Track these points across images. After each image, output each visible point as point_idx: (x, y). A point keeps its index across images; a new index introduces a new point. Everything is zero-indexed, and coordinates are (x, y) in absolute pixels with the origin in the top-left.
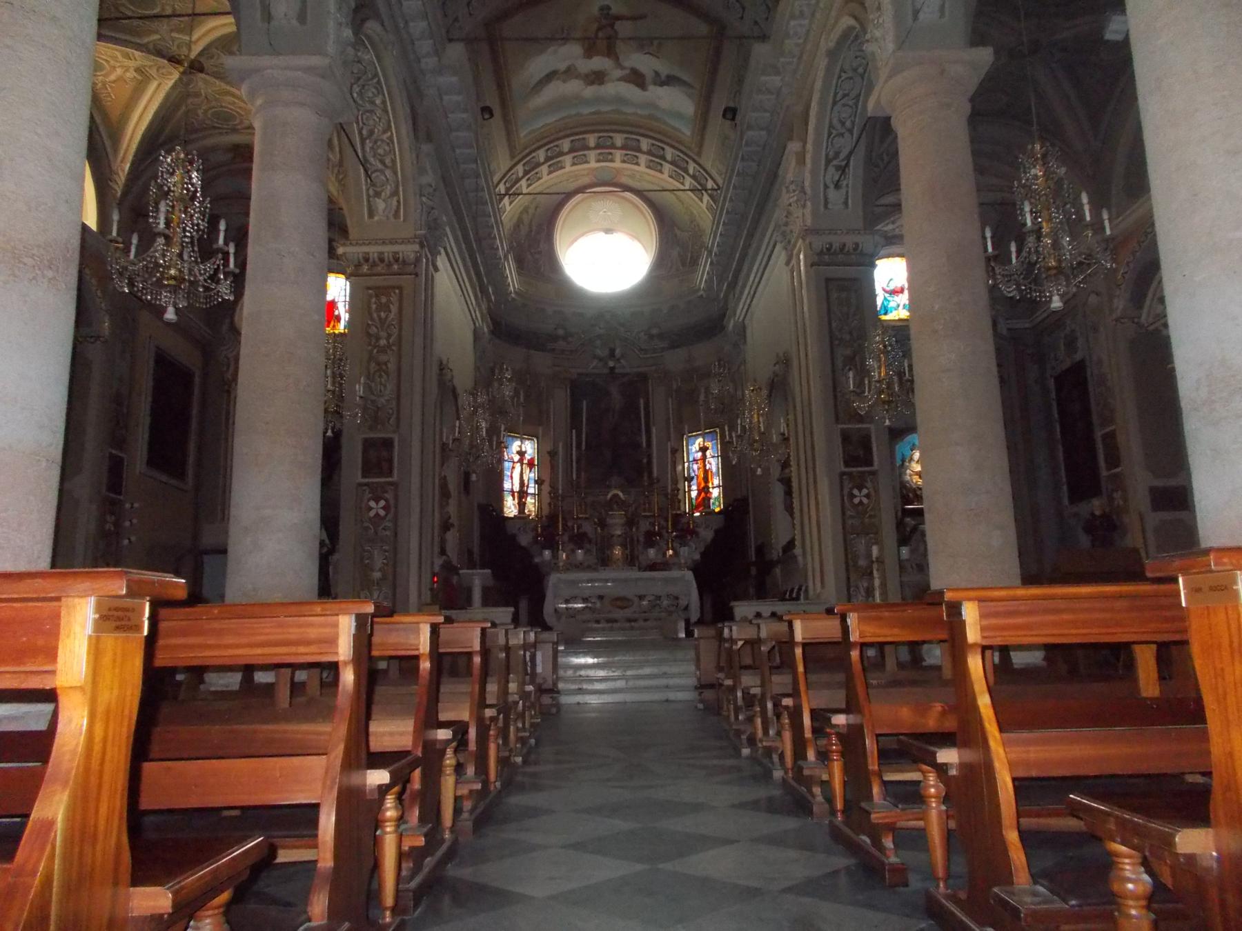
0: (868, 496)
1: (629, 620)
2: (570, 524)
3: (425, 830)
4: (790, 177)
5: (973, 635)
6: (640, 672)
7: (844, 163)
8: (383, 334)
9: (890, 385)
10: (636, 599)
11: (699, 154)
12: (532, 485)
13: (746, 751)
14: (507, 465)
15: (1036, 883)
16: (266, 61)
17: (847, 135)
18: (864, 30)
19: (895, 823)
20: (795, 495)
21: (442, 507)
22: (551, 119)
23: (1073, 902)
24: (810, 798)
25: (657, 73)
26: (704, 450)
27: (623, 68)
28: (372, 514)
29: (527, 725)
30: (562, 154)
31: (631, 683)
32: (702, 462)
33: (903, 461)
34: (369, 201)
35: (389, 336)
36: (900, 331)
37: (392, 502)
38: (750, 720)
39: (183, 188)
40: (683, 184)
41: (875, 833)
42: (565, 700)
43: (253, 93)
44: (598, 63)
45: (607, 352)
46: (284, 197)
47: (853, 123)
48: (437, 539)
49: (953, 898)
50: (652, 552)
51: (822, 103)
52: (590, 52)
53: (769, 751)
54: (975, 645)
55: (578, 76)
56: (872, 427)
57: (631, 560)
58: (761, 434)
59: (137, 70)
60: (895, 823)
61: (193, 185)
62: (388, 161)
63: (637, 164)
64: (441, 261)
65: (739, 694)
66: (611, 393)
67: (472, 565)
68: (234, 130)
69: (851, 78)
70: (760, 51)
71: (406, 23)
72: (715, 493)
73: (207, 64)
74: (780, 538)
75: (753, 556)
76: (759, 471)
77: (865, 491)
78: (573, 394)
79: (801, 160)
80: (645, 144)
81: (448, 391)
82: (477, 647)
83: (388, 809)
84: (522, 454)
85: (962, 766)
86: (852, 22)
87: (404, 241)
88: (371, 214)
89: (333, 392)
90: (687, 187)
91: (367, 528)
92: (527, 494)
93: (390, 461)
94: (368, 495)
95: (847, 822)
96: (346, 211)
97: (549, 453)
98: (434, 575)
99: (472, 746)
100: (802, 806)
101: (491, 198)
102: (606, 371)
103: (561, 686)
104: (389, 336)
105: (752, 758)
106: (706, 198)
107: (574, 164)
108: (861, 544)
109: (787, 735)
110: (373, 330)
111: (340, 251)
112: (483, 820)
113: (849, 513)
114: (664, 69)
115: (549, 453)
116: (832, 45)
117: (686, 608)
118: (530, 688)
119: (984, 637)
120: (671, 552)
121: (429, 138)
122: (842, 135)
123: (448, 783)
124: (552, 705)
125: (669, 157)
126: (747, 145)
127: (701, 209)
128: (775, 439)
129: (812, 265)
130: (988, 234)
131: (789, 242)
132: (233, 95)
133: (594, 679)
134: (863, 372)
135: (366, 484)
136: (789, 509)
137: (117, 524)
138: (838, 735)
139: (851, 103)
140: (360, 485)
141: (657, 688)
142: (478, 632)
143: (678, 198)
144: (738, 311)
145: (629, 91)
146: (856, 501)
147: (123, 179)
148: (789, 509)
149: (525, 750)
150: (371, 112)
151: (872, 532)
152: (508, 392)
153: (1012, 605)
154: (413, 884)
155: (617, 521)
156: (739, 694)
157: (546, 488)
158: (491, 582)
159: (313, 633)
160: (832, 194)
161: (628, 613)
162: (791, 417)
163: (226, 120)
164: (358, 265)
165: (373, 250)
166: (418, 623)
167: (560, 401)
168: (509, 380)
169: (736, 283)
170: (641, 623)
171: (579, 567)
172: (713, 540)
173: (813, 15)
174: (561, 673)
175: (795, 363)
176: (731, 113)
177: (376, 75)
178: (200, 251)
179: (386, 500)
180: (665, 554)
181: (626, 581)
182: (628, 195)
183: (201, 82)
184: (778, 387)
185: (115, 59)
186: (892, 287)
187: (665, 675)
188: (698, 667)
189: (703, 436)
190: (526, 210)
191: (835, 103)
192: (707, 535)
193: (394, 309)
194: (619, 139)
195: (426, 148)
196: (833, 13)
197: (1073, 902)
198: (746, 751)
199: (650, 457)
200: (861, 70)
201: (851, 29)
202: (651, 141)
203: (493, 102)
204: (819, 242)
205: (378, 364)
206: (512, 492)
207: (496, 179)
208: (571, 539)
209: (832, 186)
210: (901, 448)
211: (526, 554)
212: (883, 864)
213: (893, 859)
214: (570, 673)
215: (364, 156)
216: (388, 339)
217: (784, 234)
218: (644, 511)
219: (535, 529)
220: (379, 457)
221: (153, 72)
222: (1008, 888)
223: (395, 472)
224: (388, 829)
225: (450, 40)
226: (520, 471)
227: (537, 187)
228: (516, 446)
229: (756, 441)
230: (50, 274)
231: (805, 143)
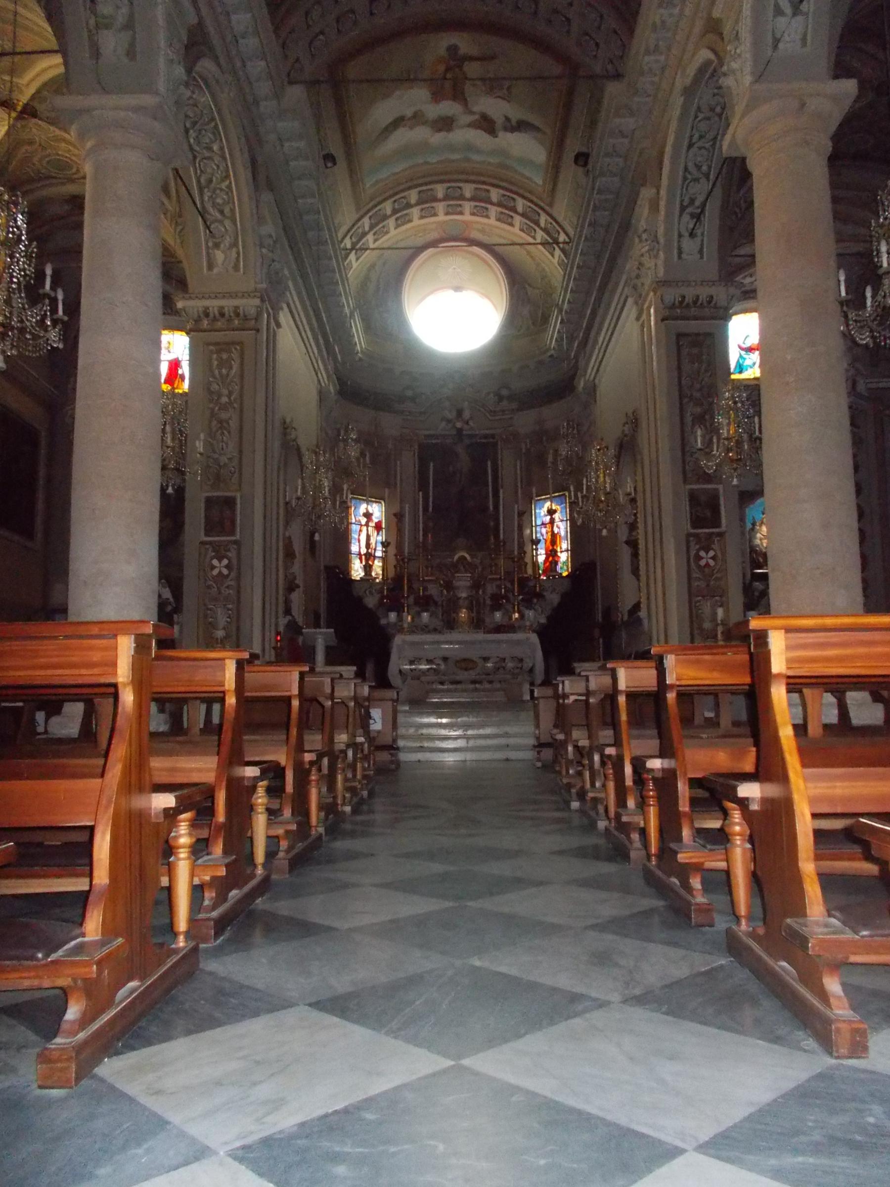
0: (713, 558)
1: (474, 682)
2: (415, 586)
3: (227, 861)
4: (643, 225)
5: (778, 665)
6: (481, 732)
7: (699, 210)
9: (739, 443)
10: (480, 663)
11: (551, 205)
12: (380, 548)
13: (575, 805)
14: (355, 528)
15: (830, 915)
16: (93, 100)
17: (703, 180)
18: (721, 64)
19: (703, 864)
20: (642, 558)
21: (286, 568)
22: (399, 168)
23: (865, 933)
24: (627, 843)
25: (508, 119)
26: (551, 512)
27: (472, 113)
28: (215, 572)
29: (359, 777)
30: (409, 206)
31: (472, 743)
32: (550, 525)
33: (754, 524)
34: (208, 254)
36: (753, 389)
37: (235, 561)
38: (580, 774)
39: (8, 232)
40: (534, 238)
41: (684, 872)
42: (403, 757)
43: (82, 136)
44: (448, 108)
45: (454, 413)
46: (119, 249)
47: (710, 167)
48: (281, 599)
49: (753, 935)
50: (498, 615)
51: (676, 148)
52: (437, 96)
53: (595, 800)
54: (779, 675)
55: (425, 123)
56: (721, 487)
57: (477, 624)
58: (607, 494)
60: (703, 864)
61: (18, 228)
62: (227, 211)
63: (487, 217)
64: (284, 317)
65: (570, 748)
66: (462, 459)
67: (317, 625)
68: (72, 181)
69: (708, 119)
70: (612, 88)
72: (563, 557)
73: (40, 107)
74: (626, 603)
75: (599, 617)
76: (604, 532)
77: (711, 553)
78: (421, 459)
79: (654, 207)
80: (495, 194)
81: (291, 449)
82: (295, 691)
83: (180, 836)
84: (368, 515)
85: (764, 801)
86: (712, 56)
88: (210, 267)
89: (173, 449)
90: (539, 241)
91: (209, 587)
92: (375, 557)
93: (233, 522)
95: (658, 866)
96: (185, 264)
97: (395, 515)
98: (278, 633)
99: (289, 788)
100: (620, 853)
101: (335, 252)
102: (454, 432)
103: (401, 743)
105: (582, 811)
106: (557, 252)
107: (422, 217)
108: (706, 608)
109: (611, 785)
110: (215, 387)
111: (180, 305)
112: (297, 862)
113: (694, 575)
114: (515, 113)
115: (395, 515)
116: (688, 81)
117: (531, 670)
118: (360, 739)
119: (788, 668)
120: (517, 615)
121: (271, 188)
122: (696, 180)
123: (260, 821)
124: (392, 762)
125: (520, 209)
126: (600, 192)
127: (551, 264)
128: (622, 499)
129: (663, 320)
130: (842, 278)
131: (640, 296)
132: (64, 140)
133: (446, 741)
134: (713, 430)
135: (210, 543)
136: (635, 571)
138: (654, 779)
139: (707, 145)
140: (203, 543)
141: (499, 748)
142: (296, 676)
143: (529, 253)
144: (589, 371)
145: (478, 137)
146: (703, 563)
148: (635, 571)
149: (355, 800)
150: (210, 158)
151: (717, 594)
152: (353, 452)
153: (821, 637)
154: (215, 914)
155: (463, 582)
156: (570, 748)
157: (392, 550)
158: (333, 642)
159: (96, 657)
160: (689, 245)
161: (472, 675)
162: (639, 478)
163: (64, 170)
164: (198, 321)
165: (214, 304)
166: (224, 659)
167: (407, 464)
168: (356, 441)
169: (587, 341)
170: (487, 686)
171: (426, 629)
172: (559, 604)
173: (669, 49)
174: (402, 731)
175: (644, 425)
176: (582, 159)
177: (213, 119)
178: (27, 297)
179: (229, 560)
180: (511, 618)
181: (473, 643)
182: (475, 249)
184: (627, 448)
186: (748, 344)
187: (506, 735)
188: (537, 726)
189: (551, 499)
190: (373, 266)
191: (690, 146)
192: (554, 598)
194: (468, 190)
195: (267, 197)
196: (690, 47)
197: (865, 933)
198: (575, 805)
199: (497, 520)
200: (718, 110)
201: (707, 63)
202: (502, 192)
203: (338, 152)
204: (671, 295)
205: (220, 422)
206: (360, 554)
207: (340, 235)
208: (416, 603)
209: (687, 234)
210: (753, 511)
211: (371, 616)
212: (689, 904)
213: (700, 899)
214: (412, 731)
215: (204, 207)
217: (635, 287)
218: (491, 573)
219: (381, 592)
220: (222, 515)
222: (801, 920)
224: (182, 856)
225: (291, 83)
226: (368, 532)
227: (383, 241)
228: (363, 508)
229: (602, 501)
231: (658, 189)
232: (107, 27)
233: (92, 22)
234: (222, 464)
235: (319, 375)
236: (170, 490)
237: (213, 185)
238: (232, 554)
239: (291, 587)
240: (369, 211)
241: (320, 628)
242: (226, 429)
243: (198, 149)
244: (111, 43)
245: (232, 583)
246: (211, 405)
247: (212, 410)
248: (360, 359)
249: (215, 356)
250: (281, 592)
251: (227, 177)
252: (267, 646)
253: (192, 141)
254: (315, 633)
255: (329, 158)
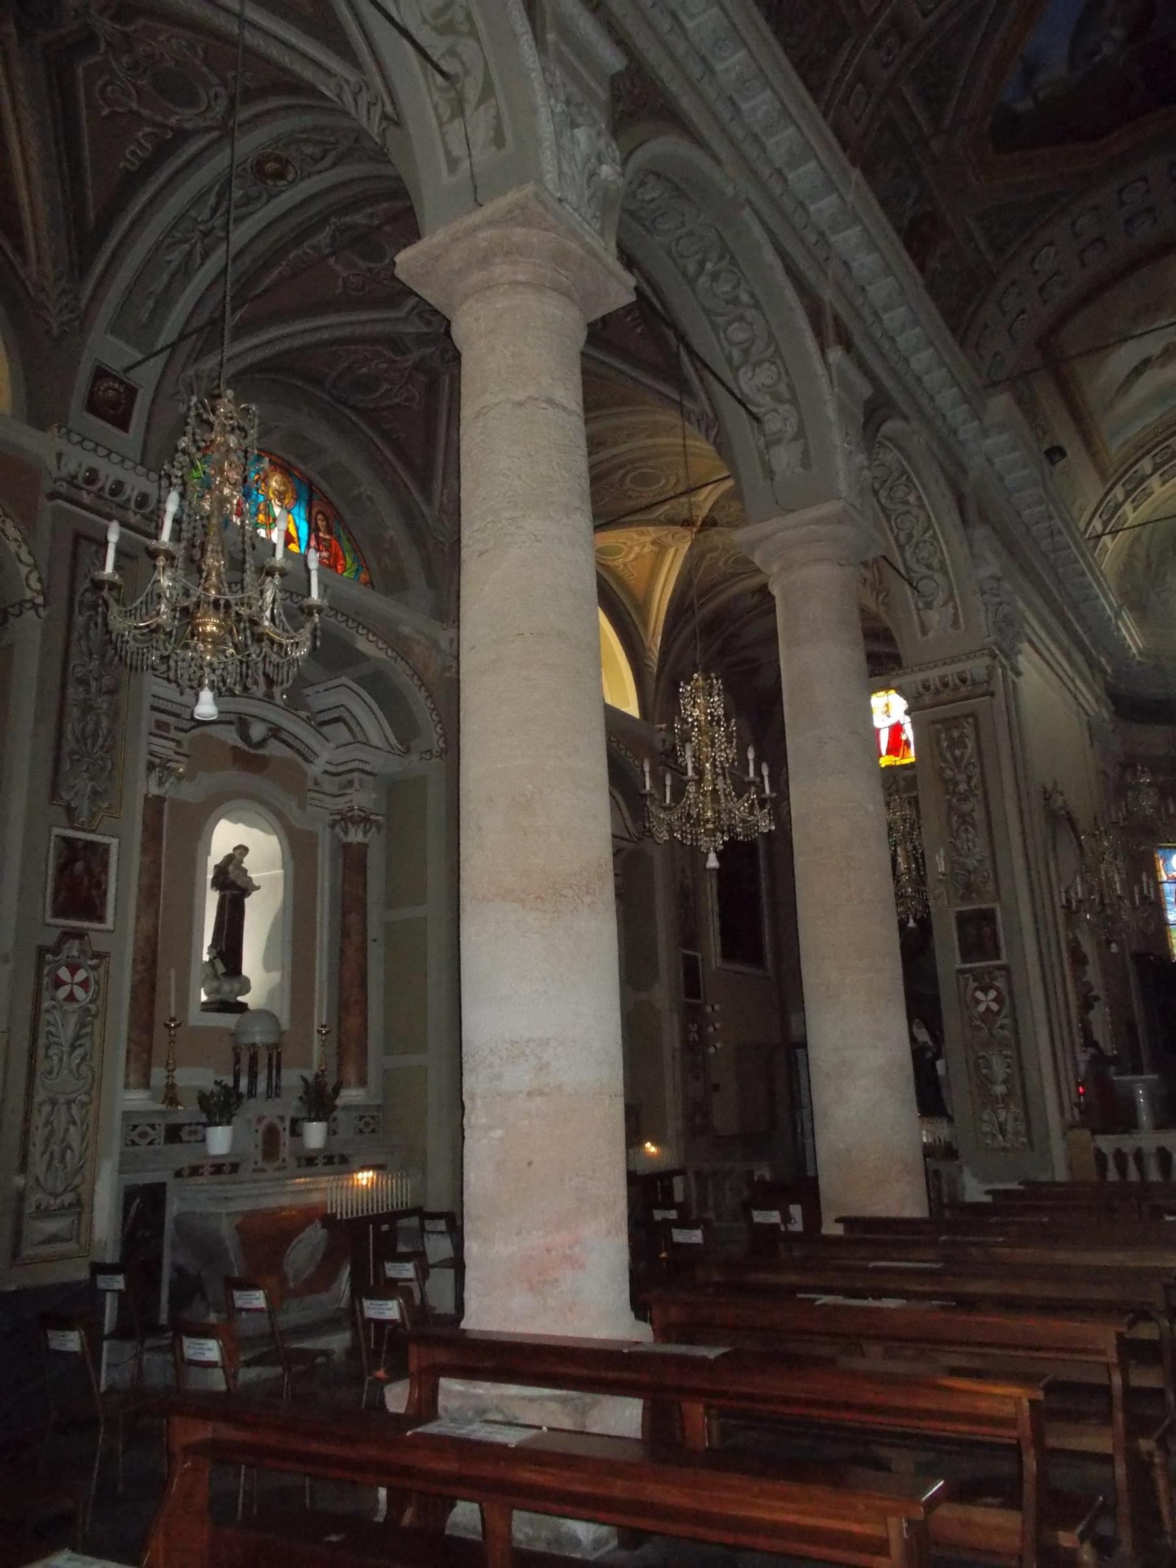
8: (962, 777)
21: (1077, 978)
28: (982, 1008)
34: (919, 615)
35: (970, 778)
37: (1005, 992)
59: (654, 543)
62: (935, 563)
67: (1137, 1070)
71: (932, 399)
81: (1060, 820)
87: (970, 655)
94: (972, 984)
104: (970, 778)
110: (949, 773)
135: (970, 970)
137: (700, 1031)
147: (657, 654)
150: (909, 512)
165: (933, 675)
177: (904, 472)
183: (716, 537)
185: (631, 539)
193: (970, 744)
215: (908, 569)
216: (968, 783)
220: (979, 935)
221: (669, 540)
223: (1003, 951)
225: (994, 384)
230: (588, 899)
232: (779, 441)
233: (762, 442)
234: (971, 869)
235: (1079, 696)
236: (911, 924)
237: (914, 540)
238: (1000, 983)
239: (1087, 1003)
240: (1120, 479)
241: (1142, 1074)
242: (969, 824)
243: (891, 507)
244: (784, 458)
245: (1006, 1021)
246: (948, 797)
247: (949, 802)
248: (1140, 663)
249: (943, 735)
250: (1074, 1011)
251: (930, 526)
252: (1066, 1105)
253: (883, 501)
254: (1132, 1082)
255: (1055, 453)
